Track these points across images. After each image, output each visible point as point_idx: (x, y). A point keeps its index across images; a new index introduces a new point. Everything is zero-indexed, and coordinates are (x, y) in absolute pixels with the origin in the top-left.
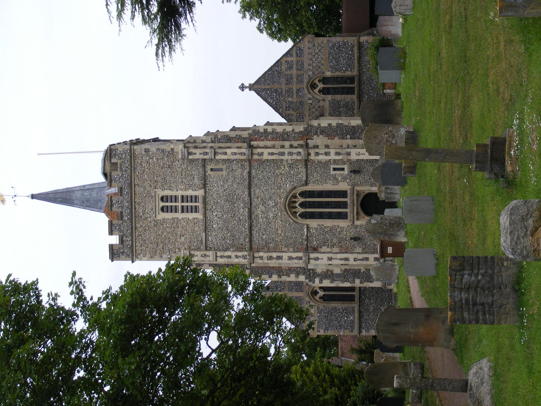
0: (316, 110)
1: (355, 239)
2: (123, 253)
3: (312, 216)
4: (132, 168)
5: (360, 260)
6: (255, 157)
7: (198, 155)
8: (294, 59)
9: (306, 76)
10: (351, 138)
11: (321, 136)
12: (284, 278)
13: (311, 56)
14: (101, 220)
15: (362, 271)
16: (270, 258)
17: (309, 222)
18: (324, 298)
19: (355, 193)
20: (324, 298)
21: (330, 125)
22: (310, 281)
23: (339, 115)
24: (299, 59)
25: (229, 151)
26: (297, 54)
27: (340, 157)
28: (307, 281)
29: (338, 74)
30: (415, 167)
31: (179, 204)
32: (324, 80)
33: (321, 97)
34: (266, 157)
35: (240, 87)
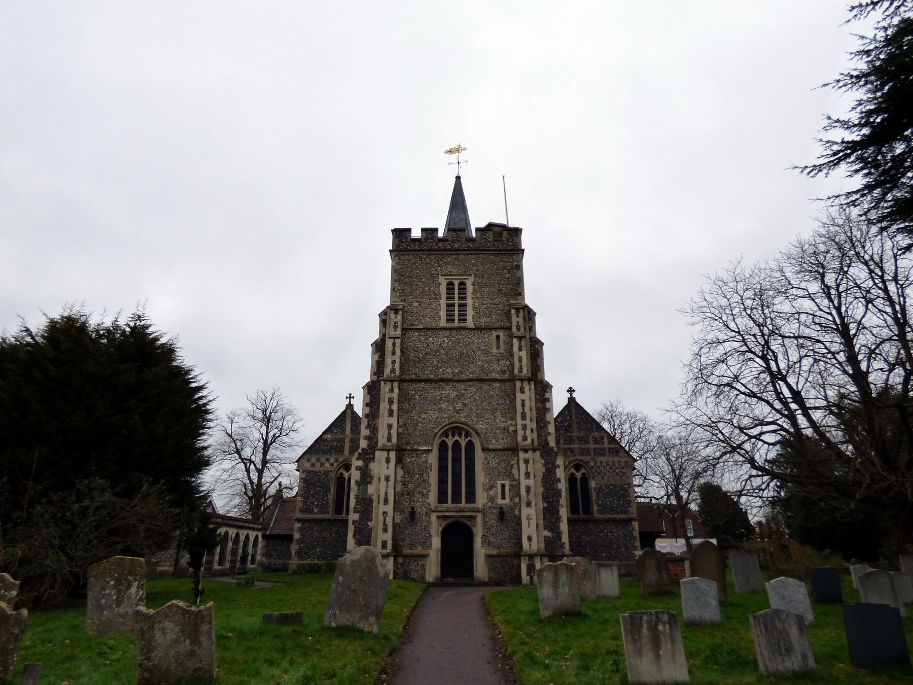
1: (413, 514)
2: (402, 241)
3: (442, 459)
4: (497, 252)
5: (385, 520)
9: (588, 459)
10: (544, 508)
11: (544, 469)
13: (610, 463)
15: (369, 523)
16: (391, 402)
17: (435, 452)
18: (341, 479)
21: (559, 480)
22: (360, 454)
24: (607, 451)
25: (523, 354)
26: (612, 449)
28: (360, 451)
29: (594, 495)
32: (585, 479)
34: (519, 397)
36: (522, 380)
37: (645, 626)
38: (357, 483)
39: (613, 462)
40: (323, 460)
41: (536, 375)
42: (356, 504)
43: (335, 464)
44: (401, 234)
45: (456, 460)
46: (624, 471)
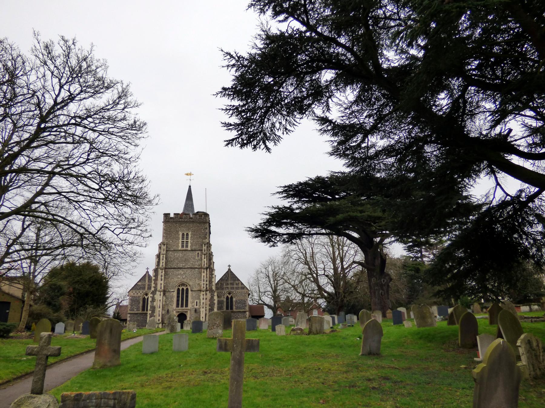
1: (168, 311)
3: (178, 293)
4: (200, 223)
6: (203, 270)
7: (204, 248)
8: (240, 286)
12: (153, 282)
14: (180, 211)
16: (162, 276)
17: (176, 292)
18: (144, 299)
20: (144, 299)
23: (218, 304)
25: (205, 260)
27: (202, 304)
29: (234, 303)
30: (226, 350)
31: (185, 240)
32: (232, 298)
33: (225, 297)
34: (203, 274)
44: (166, 215)
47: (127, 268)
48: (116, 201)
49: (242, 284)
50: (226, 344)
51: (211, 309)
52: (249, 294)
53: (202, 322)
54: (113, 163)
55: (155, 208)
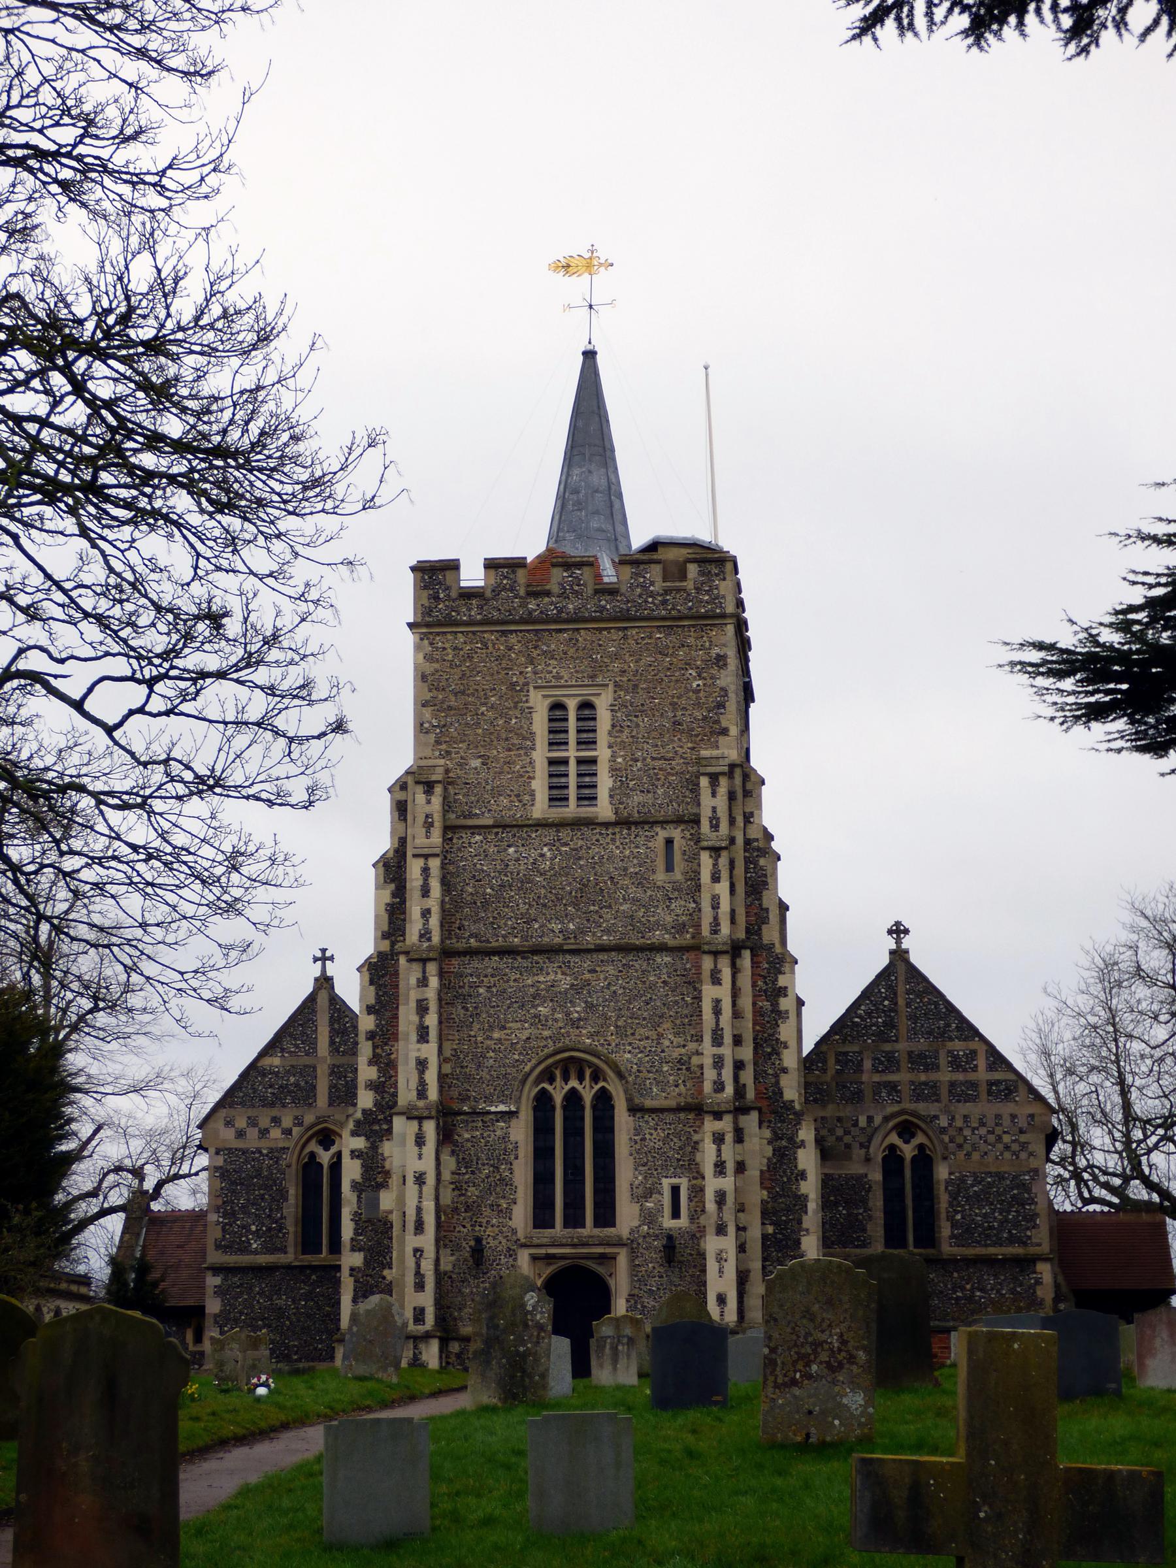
0: (839, 1139)
1: (478, 1251)
2: (436, 598)
4: (673, 622)
5: (418, 1266)
6: (707, 963)
7: (713, 802)
8: (982, 1074)
9: (931, 1109)
10: (765, 1237)
11: (769, 1151)
12: (365, 1049)
13: (991, 1122)
14: (531, 543)
15: (386, 1272)
16: (422, 1008)
18: (311, 1166)
19: (608, 1250)
21: (803, 1175)
22: (358, 1123)
23: (826, 1204)
24: (983, 1088)
25: (723, 888)
26: (997, 1083)
27: (711, 1206)
32: (924, 1161)
34: (709, 992)
35: (898, 924)
36: (716, 954)
37: (608, 1347)
38: (355, 1186)
39: (998, 1117)
40: (264, 1122)
41: (759, 933)
42: (356, 1233)
43: (296, 1131)
44: (434, 576)
45: (573, 1132)
46: (1023, 1138)
47: (186, 959)
48: (94, 489)
49: (997, 1059)
50: (916, 1492)
51: (781, 1242)
52: (1052, 1137)
53: (720, 1333)
54: (46, 211)
55: (357, 534)
